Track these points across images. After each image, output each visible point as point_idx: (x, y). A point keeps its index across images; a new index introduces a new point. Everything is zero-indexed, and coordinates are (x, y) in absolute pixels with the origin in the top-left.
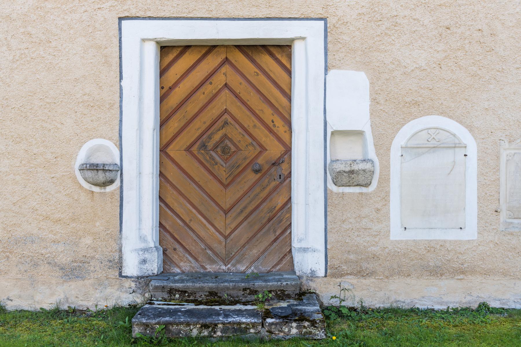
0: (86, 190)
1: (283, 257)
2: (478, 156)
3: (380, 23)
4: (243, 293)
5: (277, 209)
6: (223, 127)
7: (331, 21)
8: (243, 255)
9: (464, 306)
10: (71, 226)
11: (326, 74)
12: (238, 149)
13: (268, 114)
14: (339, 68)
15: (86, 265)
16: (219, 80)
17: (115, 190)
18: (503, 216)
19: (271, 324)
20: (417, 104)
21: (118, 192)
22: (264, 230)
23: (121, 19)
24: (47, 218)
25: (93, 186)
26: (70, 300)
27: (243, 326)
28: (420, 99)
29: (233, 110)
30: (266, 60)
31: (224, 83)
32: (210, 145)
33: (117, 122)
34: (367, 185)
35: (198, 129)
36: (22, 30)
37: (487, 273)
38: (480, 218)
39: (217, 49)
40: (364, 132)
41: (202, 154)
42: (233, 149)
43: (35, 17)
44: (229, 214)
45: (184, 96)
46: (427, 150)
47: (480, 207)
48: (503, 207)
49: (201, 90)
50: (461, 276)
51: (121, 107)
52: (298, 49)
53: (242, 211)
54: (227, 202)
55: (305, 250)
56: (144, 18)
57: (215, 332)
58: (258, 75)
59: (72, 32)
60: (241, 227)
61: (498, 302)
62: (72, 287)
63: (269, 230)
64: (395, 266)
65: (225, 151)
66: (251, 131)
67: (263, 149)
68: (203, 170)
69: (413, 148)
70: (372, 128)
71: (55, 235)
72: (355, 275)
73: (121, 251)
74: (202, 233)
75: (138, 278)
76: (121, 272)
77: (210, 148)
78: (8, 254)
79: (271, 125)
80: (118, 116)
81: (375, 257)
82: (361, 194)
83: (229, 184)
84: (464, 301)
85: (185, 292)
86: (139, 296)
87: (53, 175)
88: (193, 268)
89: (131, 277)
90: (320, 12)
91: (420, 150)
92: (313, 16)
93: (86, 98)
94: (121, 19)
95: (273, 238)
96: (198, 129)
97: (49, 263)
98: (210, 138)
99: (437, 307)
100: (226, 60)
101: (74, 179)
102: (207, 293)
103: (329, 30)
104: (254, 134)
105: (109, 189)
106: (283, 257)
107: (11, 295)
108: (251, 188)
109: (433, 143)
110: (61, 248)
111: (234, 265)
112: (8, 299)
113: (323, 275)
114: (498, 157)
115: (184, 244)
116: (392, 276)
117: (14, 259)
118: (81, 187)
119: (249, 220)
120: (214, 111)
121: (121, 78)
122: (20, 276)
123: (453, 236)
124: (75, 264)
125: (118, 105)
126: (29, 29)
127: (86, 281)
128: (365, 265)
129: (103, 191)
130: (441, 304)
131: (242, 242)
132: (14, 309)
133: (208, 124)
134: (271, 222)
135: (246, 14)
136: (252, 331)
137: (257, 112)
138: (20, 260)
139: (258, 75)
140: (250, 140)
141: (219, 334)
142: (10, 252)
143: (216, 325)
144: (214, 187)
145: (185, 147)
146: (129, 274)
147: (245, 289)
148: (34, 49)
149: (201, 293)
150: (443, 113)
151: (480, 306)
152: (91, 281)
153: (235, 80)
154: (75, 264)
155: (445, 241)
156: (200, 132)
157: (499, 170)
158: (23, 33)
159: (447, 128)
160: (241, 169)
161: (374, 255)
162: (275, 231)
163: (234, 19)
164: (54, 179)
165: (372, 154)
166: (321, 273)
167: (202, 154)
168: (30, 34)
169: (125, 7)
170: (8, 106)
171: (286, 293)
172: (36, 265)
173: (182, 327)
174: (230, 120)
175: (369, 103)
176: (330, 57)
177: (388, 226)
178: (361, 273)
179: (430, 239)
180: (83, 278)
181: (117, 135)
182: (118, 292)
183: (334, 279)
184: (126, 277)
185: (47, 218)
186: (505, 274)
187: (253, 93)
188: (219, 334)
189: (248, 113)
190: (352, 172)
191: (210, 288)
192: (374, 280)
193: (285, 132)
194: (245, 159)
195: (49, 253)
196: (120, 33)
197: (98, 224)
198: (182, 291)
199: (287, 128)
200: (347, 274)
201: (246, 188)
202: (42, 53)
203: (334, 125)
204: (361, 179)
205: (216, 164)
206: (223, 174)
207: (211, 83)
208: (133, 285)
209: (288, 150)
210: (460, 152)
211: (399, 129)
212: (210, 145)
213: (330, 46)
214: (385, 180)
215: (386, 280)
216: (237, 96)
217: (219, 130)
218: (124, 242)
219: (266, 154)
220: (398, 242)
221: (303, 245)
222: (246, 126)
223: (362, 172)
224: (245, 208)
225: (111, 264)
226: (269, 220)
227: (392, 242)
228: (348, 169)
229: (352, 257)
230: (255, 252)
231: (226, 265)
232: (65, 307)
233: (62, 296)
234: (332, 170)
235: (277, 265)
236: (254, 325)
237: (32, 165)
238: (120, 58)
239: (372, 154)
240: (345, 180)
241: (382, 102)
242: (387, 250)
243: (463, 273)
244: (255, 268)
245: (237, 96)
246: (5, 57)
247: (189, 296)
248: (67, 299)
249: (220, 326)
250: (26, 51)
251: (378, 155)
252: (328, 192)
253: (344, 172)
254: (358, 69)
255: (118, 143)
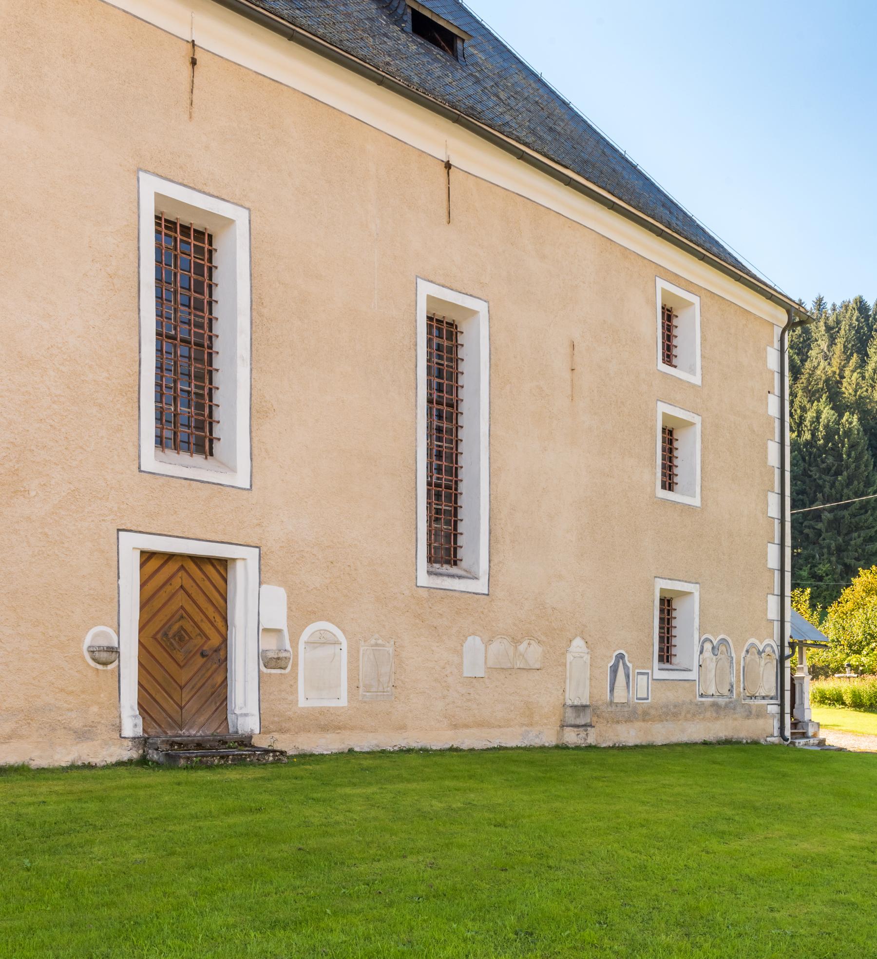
0: (92, 667)
1: (221, 723)
2: (348, 650)
3: (293, 554)
4: (217, 743)
5: (217, 686)
6: (179, 620)
7: (264, 549)
8: (194, 722)
9: (341, 751)
10: (82, 697)
11: (259, 587)
12: (191, 638)
13: (211, 612)
14: (268, 584)
15: (94, 729)
16: (177, 582)
17: (114, 668)
18: (361, 690)
19: (259, 755)
20: (314, 613)
21: (117, 669)
22: (208, 703)
23: (119, 530)
24: (62, 690)
25: (97, 664)
26: (82, 758)
27: (244, 756)
28: (316, 609)
29: (188, 608)
30: (210, 570)
31: (180, 585)
32: (171, 634)
33: (116, 613)
34: (285, 668)
35: (161, 621)
36: (40, 530)
37: (352, 729)
38: (349, 692)
39: (175, 557)
40: (283, 630)
41: (164, 640)
42: (187, 638)
43: (51, 521)
44: (184, 690)
45: (151, 593)
46: (319, 644)
47: (349, 684)
48: (361, 685)
49: (164, 590)
50: (339, 731)
51: (119, 601)
52: (239, 565)
53: (193, 688)
54: (183, 680)
55: (246, 715)
56: (136, 532)
57: (228, 761)
58: (204, 581)
59: (81, 536)
60: (193, 698)
61: (359, 748)
62: (84, 747)
63: (212, 702)
64: (301, 725)
65: (181, 639)
66: (200, 624)
67: (208, 639)
68: (165, 654)
69: (311, 643)
70: (288, 628)
71: (68, 704)
72: (278, 732)
73: (120, 717)
74: (165, 705)
75: (134, 738)
76: (120, 734)
77: (170, 636)
78: (29, 721)
79: (213, 620)
80: (117, 608)
81: (290, 719)
82: (281, 674)
83: (183, 666)
84: (340, 747)
85: (182, 744)
86: (135, 752)
87: (66, 655)
88: (158, 733)
89: (128, 738)
90: (256, 542)
91: (316, 644)
92: (252, 544)
93: (92, 592)
94: (119, 530)
95: (214, 709)
96: (161, 621)
97: (65, 728)
98: (170, 628)
99: (325, 753)
100: (182, 567)
101: (83, 658)
102: (195, 745)
103: (261, 556)
104: (202, 627)
105: (110, 667)
106: (221, 723)
107: (33, 755)
108: (199, 669)
109: (323, 640)
110: (74, 715)
111: (188, 730)
112: (31, 759)
113: (258, 732)
114: (358, 651)
115: (151, 714)
116: (300, 732)
117: (35, 725)
118: (89, 665)
119: (198, 694)
120: (173, 606)
121: (119, 578)
122: (40, 740)
123: (333, 704)
124: (86, 728)
125: (116, 600)
126: (46, 530)
127: (94, 742)
128: (284, 725)
129: (105, 668)
130: (327, 750)
131: (193, 711)
132: (36, 767)
133: (168, 617)
134: (213, 696)
135: (208, 537)
136: (248, 759)
137: (204, 610)
138: (40, 726)
139: (204, 581)
140: (198, 631)
141: (230, 762)
142: (32, 720)
143: (228, 756)
144: (172, 667)
145: (152, 634)
146: (127, 736)
147: (219, 741)
148: (50, 548)
149: (191, 745)
150: (328, 620)
151: (867, 356)
152: (99, 742)
153: (188, 584)
154: (86, 728)
155: (330, 707)
156: (163, 623)
157: (359, 660)
158: (41, 533)
159: (331, 631)
160: (192, 654)
161: (290, 717)
162: (216, 703)
163: (199, 540)
164: (67, 658)
165: (288, 646)
166: (257, 731)
167: (164, 640)
168: (47, 535)
169: (123, 522)
170: (27, 594)
171: (244, 743)
172: (54, 729)
173: (209, 759)
174: (185, 615)
175: (286, 610)
176: (262, 575)
177: (297, 697)
178: (282, 731)
179: (321, 706)
180: (93, 740)
181: (116, 624)
182: (120, 750)
183: (265, 735)
184: (124, 738)
185: (62, 690)
186: (362, 729)
187: (201, 594)
188: (230, 762)
189: (197, 610)
190: (278, 658)
191: (198, 740)
192: (288, 735)
193: (223, 626)
194: (195, 646)
195: (65, 719)
196: (118, 542)
197: (102, 695)
198: (179, 744)
199: (223, 623)
200: (273, 731)
201: (196, 670)
202: (56, 551)
203: (265, 624)
204: (282, 664)
205: (175, 649)
206: (180, 657)
207: (171, 584)
208: (130, 744)
209: (225, 640)
210: (338, 647)
211: (304, 630)
212: (171, 634)
213: (262, 567)
214: (295, 665)
215: (296, 735)
216: (189, 596)
217: (176, 622)
218: (122, 710)
219: (209, 642)
220: (303, 708)
221: (244, 711)
222: (196, 620)
223: (284, 659)
224: (195, 685)
225: (113, 727)
226: (212, 694)
227: (300, 708)
228: (276, 656)
229: (276, 719)
230: (202, 719)
231: (181, 730)
232: (80, 763)
233: (76, 755)
234: (262, 656)
235: (217, 729)
236: (249, 756)
237: (48, 646)
238: (118, 561)
239: (288, 646)
240: (273, 663)
241: (294, 610)
242: (296, 714)
243: (340, 729)
244: (203, 732)
245: (189, 596)
246: (25, 552)
247: (184, 747)
248: (80, 757)
249: (231, 757)
250: (43, 549)
251: (291, 647)
252: (261, 673)
253: (274, 658)
254: (279, 586)
255: (117, 631)
